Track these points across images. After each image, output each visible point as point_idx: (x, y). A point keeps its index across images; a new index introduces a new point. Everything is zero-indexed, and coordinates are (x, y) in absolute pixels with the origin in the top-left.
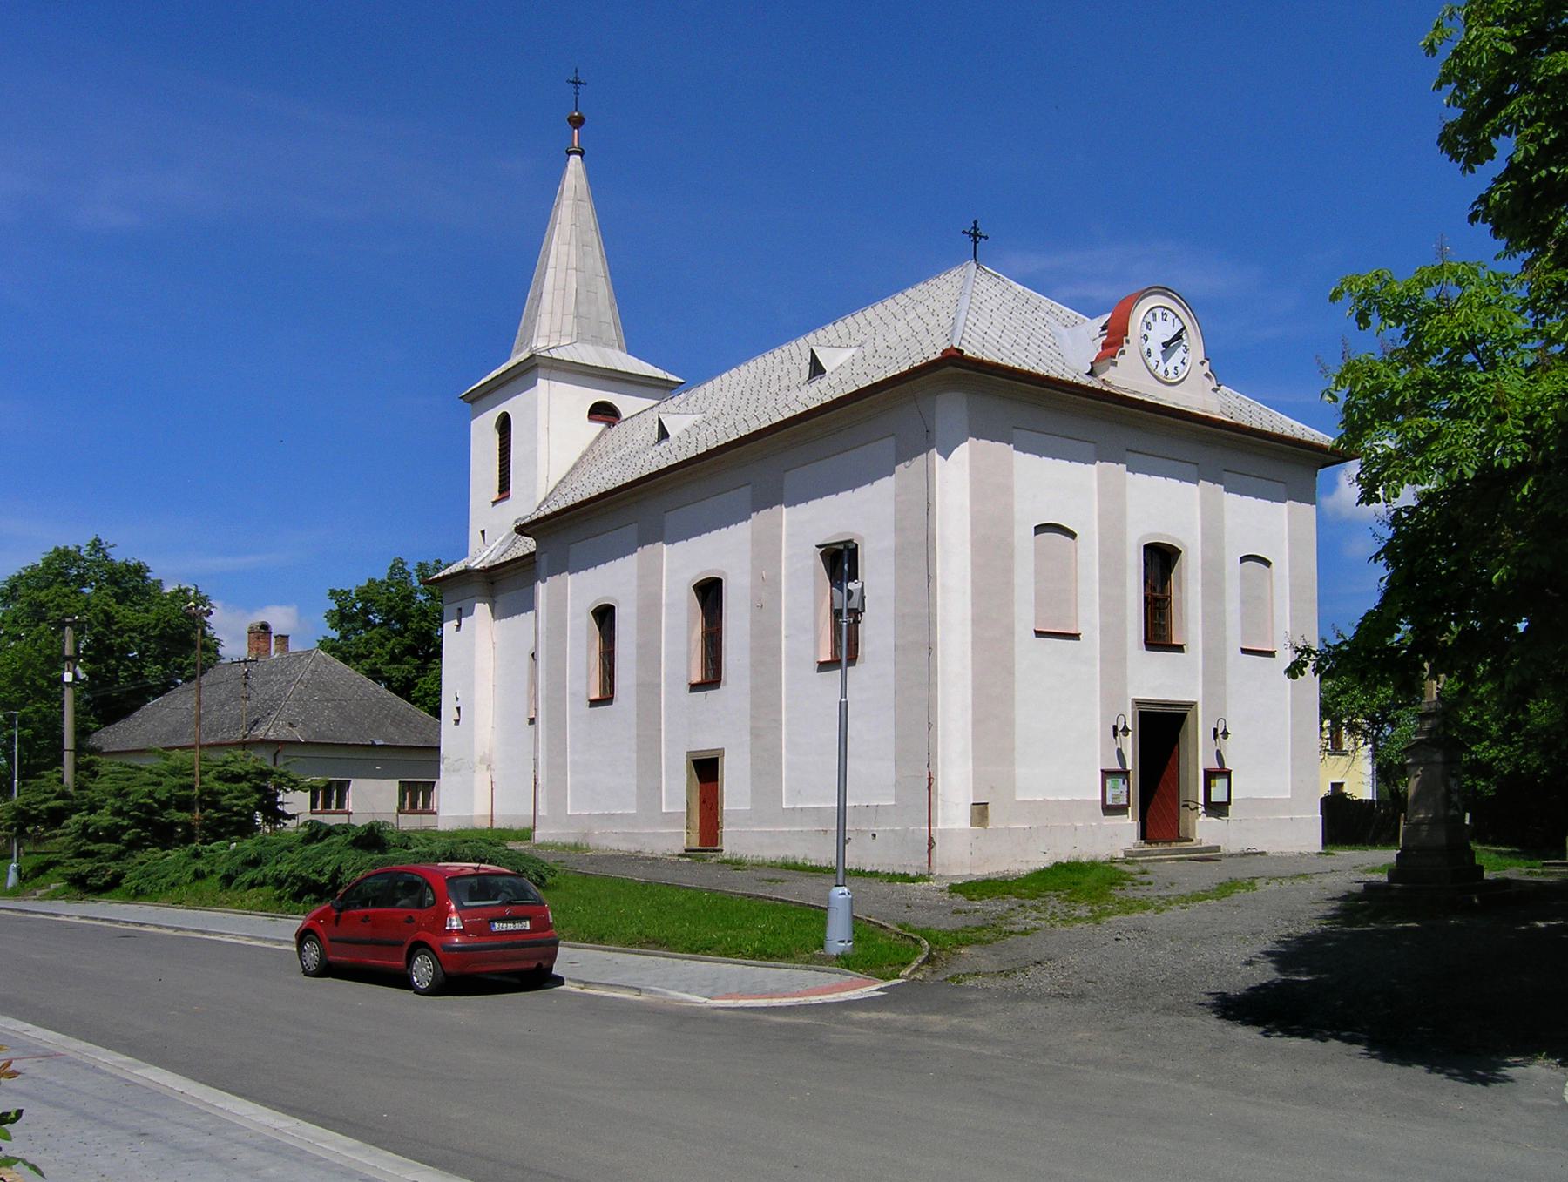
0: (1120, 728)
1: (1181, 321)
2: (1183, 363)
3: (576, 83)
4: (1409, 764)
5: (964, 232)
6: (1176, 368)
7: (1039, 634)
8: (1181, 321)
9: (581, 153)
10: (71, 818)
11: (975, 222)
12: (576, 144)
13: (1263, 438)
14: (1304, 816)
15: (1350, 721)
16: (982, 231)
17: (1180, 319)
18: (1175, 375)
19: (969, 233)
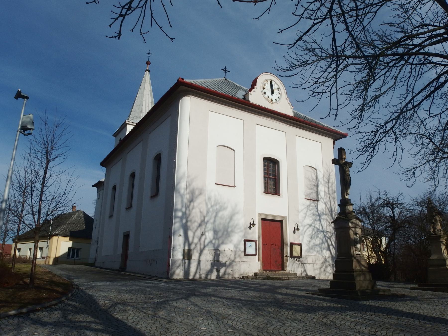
0: (296, 228)
1: (278, 85)
2: (278, 98)
3: (149, 54)
4: (388, 245)
5: (229, 72)
6: (276, 99)
7: (216, 184)
8: (278, 85)
9: (149, 71)
10: (174, 262)
11: (225, 67)
12: (148, 69)
13: (279, 116)
14: (424, 283)
15: (400, 238)
16: (228, 69)
17: (277, 84)
18: (275, 102)
19: (227, 71)
